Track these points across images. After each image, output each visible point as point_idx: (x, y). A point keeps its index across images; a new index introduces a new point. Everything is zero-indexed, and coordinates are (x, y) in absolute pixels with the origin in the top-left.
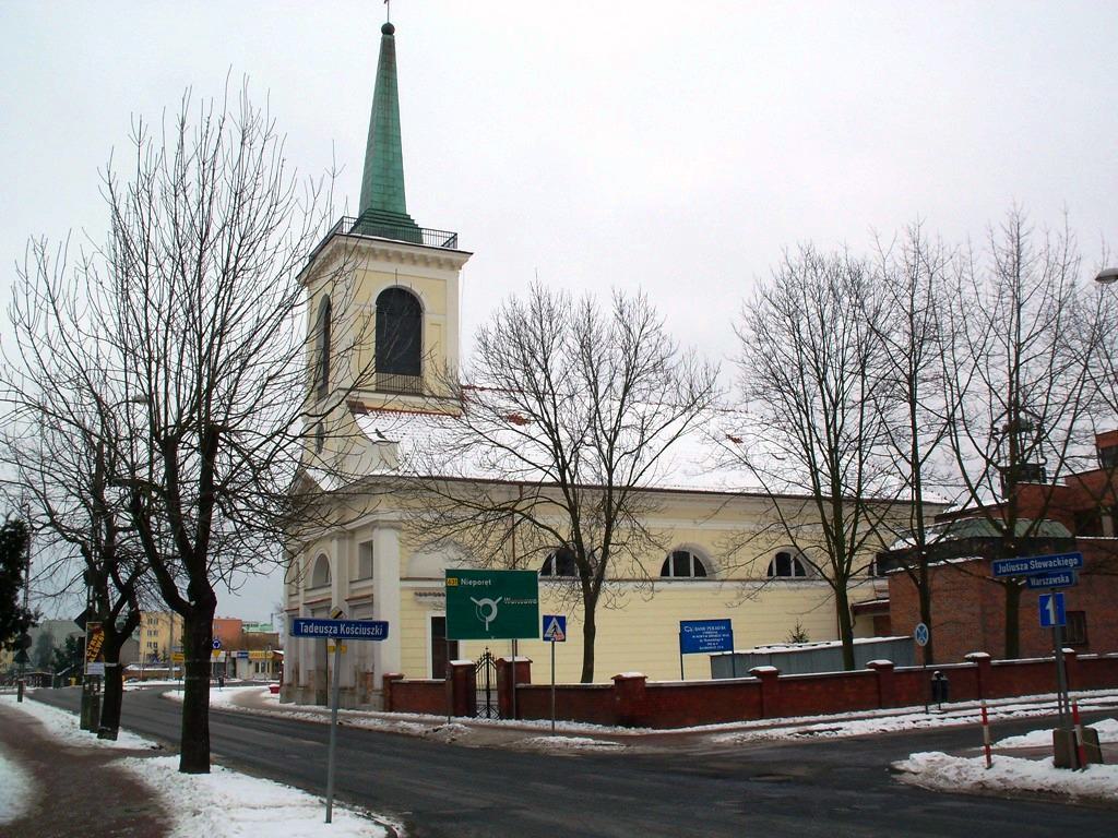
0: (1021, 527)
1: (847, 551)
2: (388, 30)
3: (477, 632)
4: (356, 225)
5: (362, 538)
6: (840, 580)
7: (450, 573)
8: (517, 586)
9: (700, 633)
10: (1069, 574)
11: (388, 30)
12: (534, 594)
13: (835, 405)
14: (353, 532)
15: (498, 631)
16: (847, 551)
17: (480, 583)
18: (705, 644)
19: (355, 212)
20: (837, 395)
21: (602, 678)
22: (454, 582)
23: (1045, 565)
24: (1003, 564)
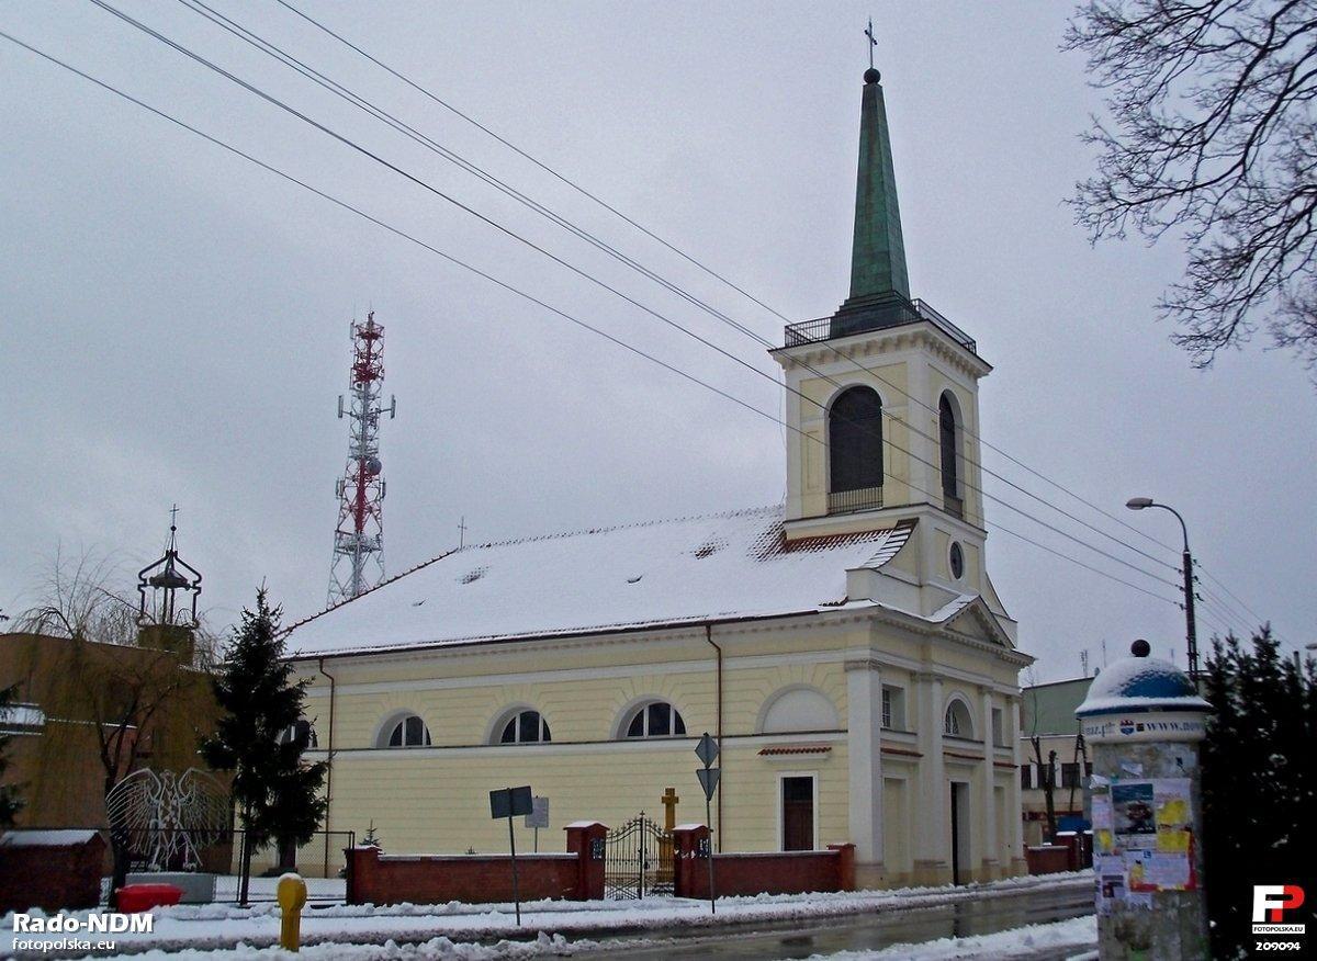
2: (872, 77)
11: (872, 77)
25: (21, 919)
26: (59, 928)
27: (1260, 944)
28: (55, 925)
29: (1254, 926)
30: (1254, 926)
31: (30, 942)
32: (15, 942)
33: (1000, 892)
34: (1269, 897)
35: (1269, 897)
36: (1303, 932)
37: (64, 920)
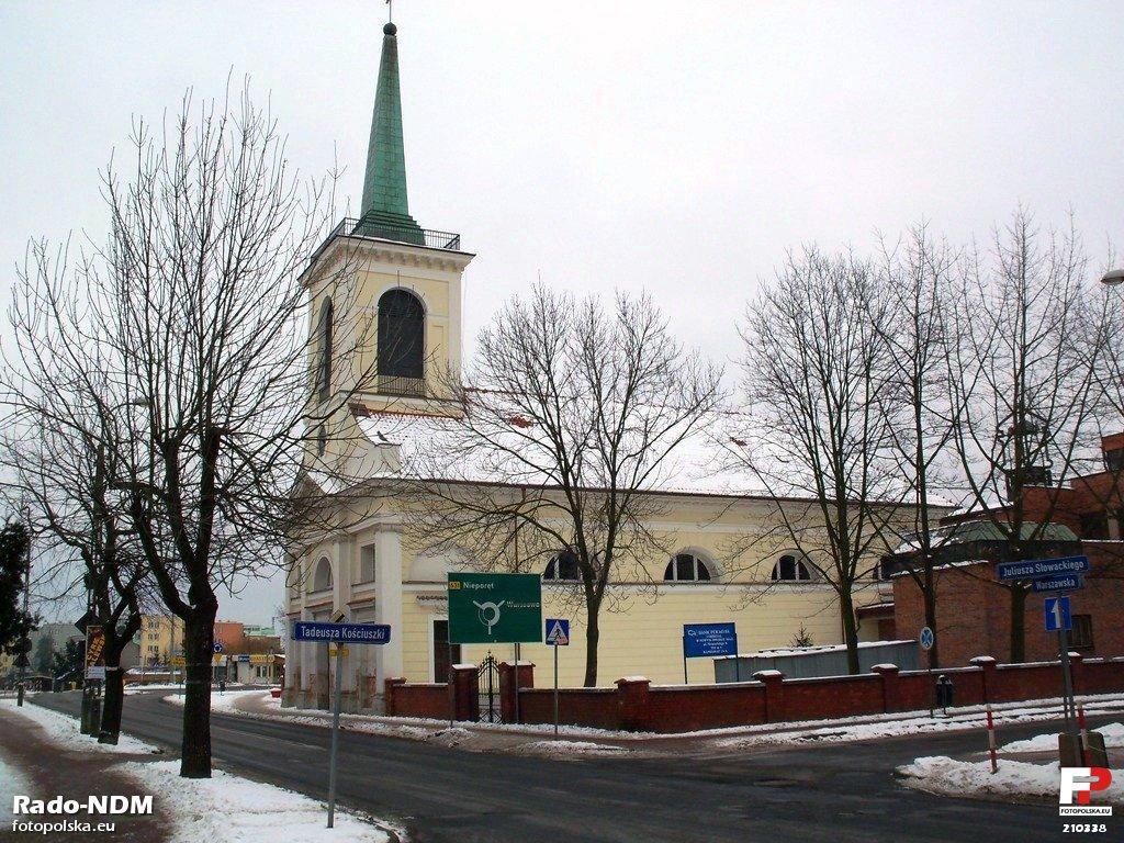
0: (1027, 530)
1: (851, 554)
2: (390, 30)
3: (480, 636)
4: (358, 226)
5: (364, 541)
6: (845, 584)
7: (452, 577)
8: (520, 589)
9: (704, 636)
10: (1075, 578)
11: (390, 30)
12: (536, 596)
13: (840, 407)
14: (355, 535)
15: (501, 635)
16: (851, 554)
17: (482, 586)
18: (708, 648)
19: (356, 213)
20: (842, 397)
21: (606, 682)
22: (456, 585)
23: (1051, 568)
24: (1009, 567)
25: (22, 801)
26: (59, 811)
27: (1067, 826)
28: (55, 807)
29: (1061, 808)
30: (1061, 808)
31: (30, 824)
32: (15, 824)
33: (162, 403)
34: (1077, 780)
35: (1077, 780)
36: (1110, 814)
37: (64, 802)
